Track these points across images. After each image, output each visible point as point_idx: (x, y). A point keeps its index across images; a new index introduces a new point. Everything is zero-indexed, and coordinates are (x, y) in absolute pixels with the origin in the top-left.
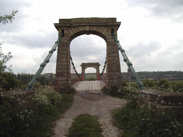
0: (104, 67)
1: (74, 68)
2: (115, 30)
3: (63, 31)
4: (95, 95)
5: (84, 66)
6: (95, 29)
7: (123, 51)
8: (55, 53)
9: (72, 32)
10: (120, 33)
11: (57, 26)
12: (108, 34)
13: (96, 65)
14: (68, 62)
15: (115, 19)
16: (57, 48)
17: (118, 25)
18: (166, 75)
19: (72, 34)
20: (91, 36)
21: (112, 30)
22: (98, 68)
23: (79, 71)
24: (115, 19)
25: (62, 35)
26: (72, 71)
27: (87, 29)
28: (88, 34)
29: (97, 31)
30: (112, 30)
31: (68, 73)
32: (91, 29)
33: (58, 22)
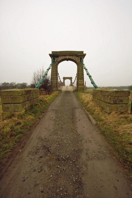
0: (75, 79)
1: (60, 79)
2: (82, 59)
3: (54, 58)
4: (18, 104)
5: (65, 78)
6: (71, 57)
7: (86, 70)
8: (50, 70)
9: (60, 58)
10: (85, 61)
11: (50, 55)
12: (78, 61)
13: (71, 78)
14: (57, 76)
15: (83, 52)
16: (51, 68)
17: (85, 55)
18: (64, 57)
19: (59, 60)
20: (69, 61)
21: (81, 58)
22: (72, 79)
23: (62, 81)
24: (83, 52)
25: (53, 61)
26: (59, 80)
27: (67, 57)
28: (67, 60)
29: (71, 58)
30: (81, 58)
31: (57, 82)
32: (70, 58)
33: (51, 53)
